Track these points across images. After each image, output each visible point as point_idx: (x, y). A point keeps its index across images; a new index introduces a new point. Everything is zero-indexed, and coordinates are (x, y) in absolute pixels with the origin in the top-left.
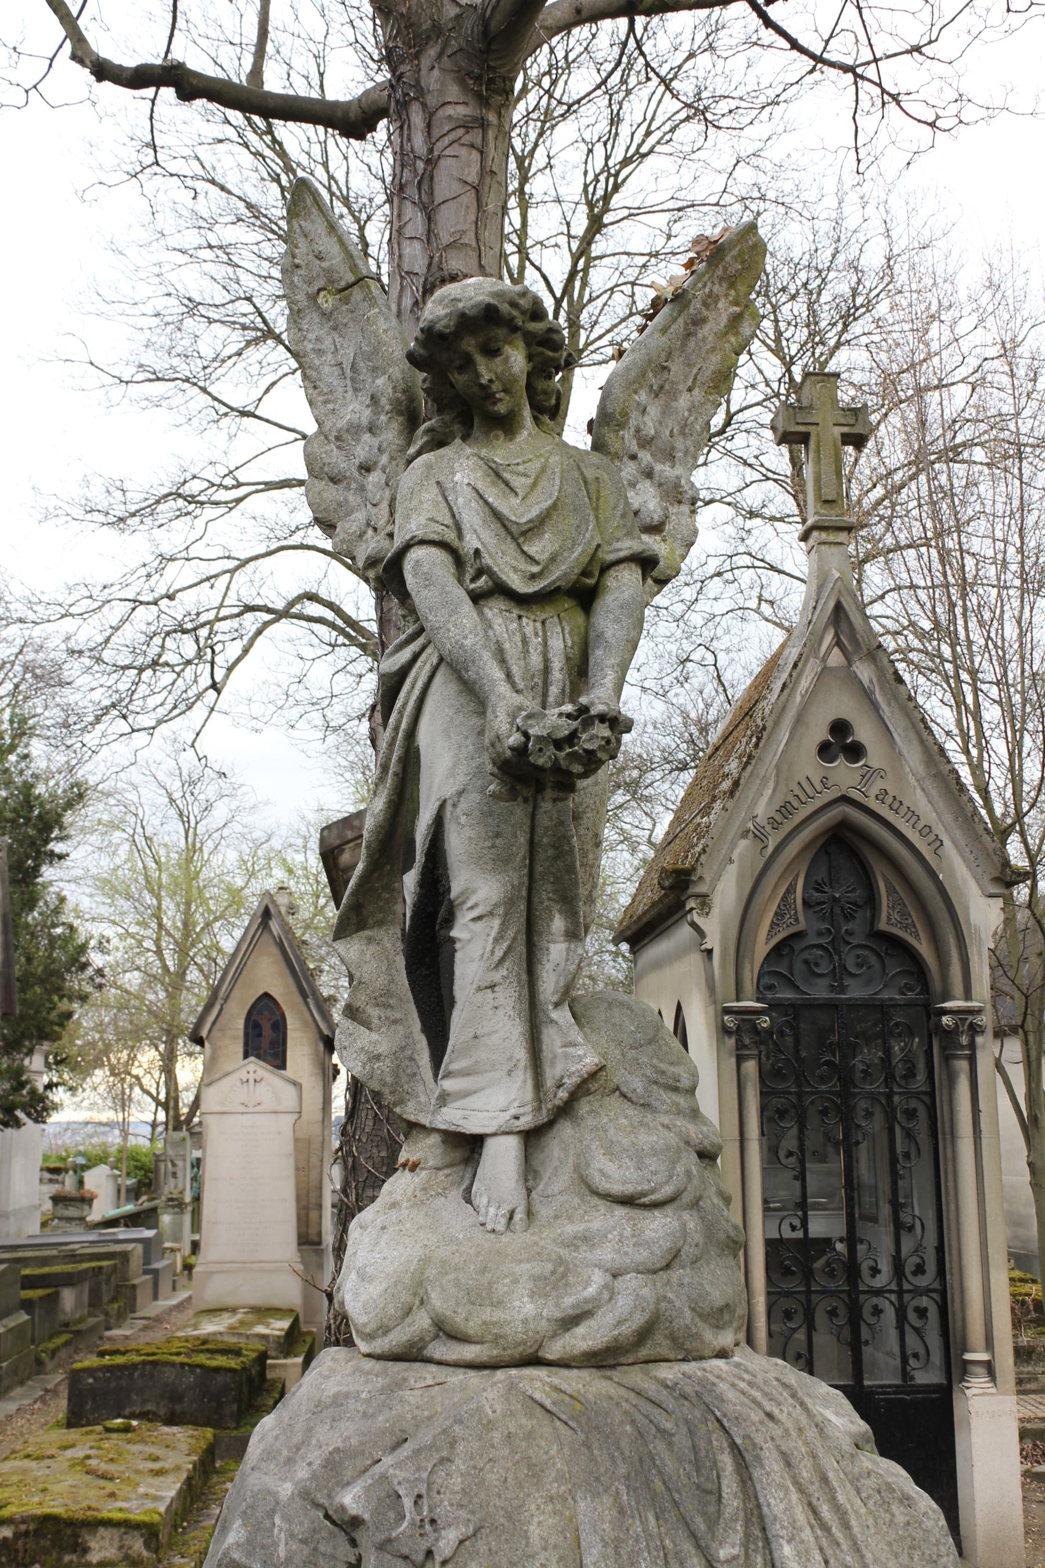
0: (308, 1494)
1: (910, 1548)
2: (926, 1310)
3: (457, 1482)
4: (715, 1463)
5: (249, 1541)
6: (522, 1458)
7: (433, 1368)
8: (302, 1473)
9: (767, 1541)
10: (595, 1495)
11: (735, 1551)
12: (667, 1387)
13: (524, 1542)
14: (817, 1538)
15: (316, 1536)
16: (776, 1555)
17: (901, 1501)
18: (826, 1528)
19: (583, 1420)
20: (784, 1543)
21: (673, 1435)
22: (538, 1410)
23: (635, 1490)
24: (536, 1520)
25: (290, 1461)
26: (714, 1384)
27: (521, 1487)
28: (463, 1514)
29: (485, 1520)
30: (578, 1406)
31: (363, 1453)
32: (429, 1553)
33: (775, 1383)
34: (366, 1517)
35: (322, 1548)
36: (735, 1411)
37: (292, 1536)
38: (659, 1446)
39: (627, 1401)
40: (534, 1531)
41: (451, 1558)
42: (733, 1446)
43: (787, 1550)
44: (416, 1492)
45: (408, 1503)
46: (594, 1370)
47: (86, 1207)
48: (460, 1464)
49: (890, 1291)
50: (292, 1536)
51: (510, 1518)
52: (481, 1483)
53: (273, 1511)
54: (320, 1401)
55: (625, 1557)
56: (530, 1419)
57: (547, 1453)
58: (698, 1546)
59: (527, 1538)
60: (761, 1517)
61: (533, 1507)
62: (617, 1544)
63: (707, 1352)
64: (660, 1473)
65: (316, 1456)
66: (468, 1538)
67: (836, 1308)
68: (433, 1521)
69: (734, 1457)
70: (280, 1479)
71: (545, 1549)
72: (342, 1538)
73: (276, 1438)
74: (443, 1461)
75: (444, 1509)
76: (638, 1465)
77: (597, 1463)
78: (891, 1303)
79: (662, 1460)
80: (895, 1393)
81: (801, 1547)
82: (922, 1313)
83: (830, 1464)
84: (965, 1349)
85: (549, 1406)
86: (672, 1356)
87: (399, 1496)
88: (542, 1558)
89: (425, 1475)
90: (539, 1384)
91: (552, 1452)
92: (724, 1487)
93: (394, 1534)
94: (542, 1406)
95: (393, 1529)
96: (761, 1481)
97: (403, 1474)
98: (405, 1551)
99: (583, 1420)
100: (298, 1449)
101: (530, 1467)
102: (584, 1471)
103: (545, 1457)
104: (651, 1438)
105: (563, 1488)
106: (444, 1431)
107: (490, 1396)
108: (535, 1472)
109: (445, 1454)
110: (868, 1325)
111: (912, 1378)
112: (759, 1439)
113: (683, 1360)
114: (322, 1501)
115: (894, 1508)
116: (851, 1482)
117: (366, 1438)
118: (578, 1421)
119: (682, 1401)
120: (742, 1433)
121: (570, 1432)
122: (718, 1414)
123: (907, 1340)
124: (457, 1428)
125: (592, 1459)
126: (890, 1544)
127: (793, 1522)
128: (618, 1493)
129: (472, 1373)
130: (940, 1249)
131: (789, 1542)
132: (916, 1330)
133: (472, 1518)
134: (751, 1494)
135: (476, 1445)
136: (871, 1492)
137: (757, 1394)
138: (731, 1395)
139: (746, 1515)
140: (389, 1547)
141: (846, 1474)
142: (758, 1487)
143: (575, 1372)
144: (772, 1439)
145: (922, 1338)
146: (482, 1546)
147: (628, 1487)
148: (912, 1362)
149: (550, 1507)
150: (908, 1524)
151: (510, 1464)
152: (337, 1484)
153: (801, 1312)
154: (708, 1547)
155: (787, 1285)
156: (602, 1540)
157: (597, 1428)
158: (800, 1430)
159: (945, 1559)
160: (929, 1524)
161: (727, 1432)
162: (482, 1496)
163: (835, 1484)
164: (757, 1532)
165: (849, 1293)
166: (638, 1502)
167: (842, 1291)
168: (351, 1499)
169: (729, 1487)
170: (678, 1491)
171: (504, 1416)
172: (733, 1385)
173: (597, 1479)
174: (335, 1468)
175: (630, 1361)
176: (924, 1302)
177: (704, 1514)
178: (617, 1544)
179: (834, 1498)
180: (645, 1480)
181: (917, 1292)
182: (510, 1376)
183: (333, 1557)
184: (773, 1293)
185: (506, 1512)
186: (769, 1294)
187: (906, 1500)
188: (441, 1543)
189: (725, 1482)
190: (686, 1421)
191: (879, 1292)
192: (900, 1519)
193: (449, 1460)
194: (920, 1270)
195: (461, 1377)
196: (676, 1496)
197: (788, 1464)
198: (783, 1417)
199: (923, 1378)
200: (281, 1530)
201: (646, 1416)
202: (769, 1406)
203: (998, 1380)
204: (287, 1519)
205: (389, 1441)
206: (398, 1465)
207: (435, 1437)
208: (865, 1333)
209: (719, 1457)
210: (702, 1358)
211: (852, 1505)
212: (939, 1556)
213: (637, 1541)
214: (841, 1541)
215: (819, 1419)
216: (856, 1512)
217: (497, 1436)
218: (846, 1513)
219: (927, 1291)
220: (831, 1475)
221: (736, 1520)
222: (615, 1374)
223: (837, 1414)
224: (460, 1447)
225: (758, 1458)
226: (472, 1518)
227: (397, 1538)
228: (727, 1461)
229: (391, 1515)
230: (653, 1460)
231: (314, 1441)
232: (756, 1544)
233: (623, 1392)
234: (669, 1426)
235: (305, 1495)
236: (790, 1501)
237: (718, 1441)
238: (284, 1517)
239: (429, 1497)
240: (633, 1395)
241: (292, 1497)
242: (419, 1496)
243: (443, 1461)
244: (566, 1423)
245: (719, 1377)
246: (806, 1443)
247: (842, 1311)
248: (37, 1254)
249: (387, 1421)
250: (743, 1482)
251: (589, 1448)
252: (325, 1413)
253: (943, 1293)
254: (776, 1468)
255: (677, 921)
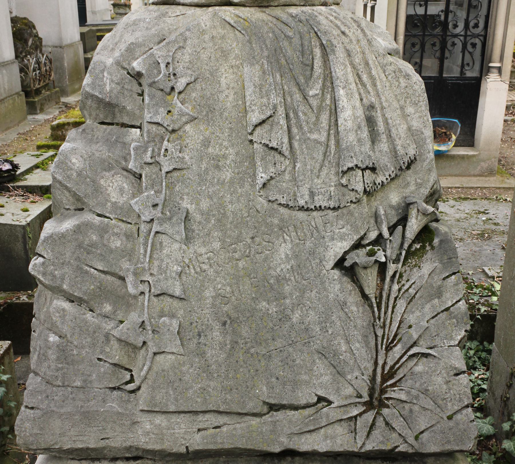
0: (119, 63)
1: (406, 98)
2: (476, 44)
3: (187, 58)
4: (312, 52)
5: (93, 83)
6: (219, 48)
7: (180, 7)
8: (117, 54)
9: (333, 88)
10: (252, 65)
11: (317, 92)
12: (293, 16)
13: (218, 85)
14: (358, 89)
15: (123, 82)
16: (336, 94)
17: (405, 77)
18: (364, 85)
19: (249, 30)
20: (341, 89)
21: (292, 38)
22: (228, 26)
23: (271, 63)
24: (224, 76)
25: (113, 49)
26: (316, 16)
27: (218, 61)
28: (189, 72)
29: (200, 75)
30: (247, 24)
31: (144, 45)
32: (173, 89)
33: (350, 19)
34: (144, 72)
35: (126, 87)
36: (325, 29)
37: (112, 81)
38: (285, 44)
39: (271, 22)
40: (223, 81)
41: (183, 91)
42: (322, 45)
43: (342, 92)
44: (167, 61)
45: (163, 66)
46: (257, 8)
47: (128, 9)
48: (188, 50)
49: (461, 35)
50: (112, 81)
51: (212, 75)
52: (198, 58)
53: (103, 71)
54: (127, 24)
55: (264, 93)
56: (224, 30)
57: (231, 46)
58: (300, 89)
59: (220, 84)
60: (331, 77)
61: (223, 70)
62: (261, 87)
63: (317, 2)
64: (284, 56)
65: (123, 47)
66: (191, 83)
67: (435, 43)
68: (174, 75)
69: (322, 50)
70: (108, 57)
71: (228, 89)
72: (135, 82)
73: (109, 41)
74: (180, 48)
75: (180, 69)
76: (273, 52)
77: (254, 50)
78: (461, 40)
79: (286, 50)
80: (456, 80)
81: (349, 92)
82: (474, 45)
83: (371, 58)
84: (490, 62)
85: (232, 23)
86: (298, 3)
87: (159, 63)
88: (226, 92)
89: (171, 54)
90: (229, 13)
91: (233, 46)
92: (315, 64)
93: (156, 80)
94: (229, 24)
95: (156, 77)
96: (333, 61)
97: (161, 53)
98: (161, 87)
99: (249, 30)
100: (116, 44)
101: (222, 52)
102: (248, 54)
103: (230, 48)
104: (281, 39)
105: (238, 62)
106: (181, 34)
107: (204, 19)
108: (225, 54)
109: (181, 44)
110: (449, 50)
111: (465, 74)
112: (335, 42)
113: (303, 6)
114: (126, 66)
115: (401, 80)
116: (382, 67)
117: (146, 38)
118: (246, 31)
119: (299, 23)
120: (326, 39)
121: (242, 36)
122: (316, 29)
123: (465, 57)
124: (187, 33)
125: (252, 48)
126: (396, 96)
127: (347, 81)
128: (263, 64)
129: (198, 9)
130: (487, 17)
131: (343, 88)
132: (470, 53)
133: (194, 74)
134: (328, 67)
135: (197, 41)
136: (390, 72)
137: (339, 23)
138: (324, 21)
139: (324, 76)
140: (154, 85)
141: (379, 63)
142: (331, 63)
143: (248, 8)
144: (343, 43)
145: (472, 57)
146: (198, 86)
147: (268, 61)
148: (467, 68)
149: (231, 70)
150: (407, 87)
151: (212, 51)
152: (133, 58)
153: (419, 43)
154: (304, 90)
155: (414, 32)
156: (254, 85)
157: (255, 34)
158: (358, 41)
159: (422, 103)
160: (416, 87)
161: (319, 38)
162: (199, 64)
163: (372, 66)
164: (329, 84)
165: (442, 36)
166: (272, 68)
167: (439, 35)
168: (137, 65)
169: (317, 63)
170: (292, 64)
171: (211, 28)
172: (327, 18)
173: (254, 58)
174: (131, 51)
175: (276, 4)
176: (477, 41)
177: (304, 75)
178: (261, 87)
179: (370, 73)
180: (276, 59)
181: (474, 36)
182: (215, 10)
183: (131, 90)
184: (408, 35)
185: (210, 72)
186: (406, 36)
187: (407, 76)
188: (178, 84)
189: (316, 61)
190: (300, 33)
191: (456, 36)
192: (403, 85)
193: (183, 47)
194: (476, 26)
195: (193, 11)
196: (291, 66)
197: (349, 55)
198: (350, 34)
199: (469, 74)
200: (107, 78)
201: (280, 30)
202: (343, 28)
203: (503, 75)
204: (110, 73)
205: (157, 40)
206: (159, 49)
207: (176, 37)
208: (447, 54)
209: (314, 50)
210: (313, 5)
211: (379, 77)
212: (418, 101)
213: (270, 86)
214: (371, 91)
215: (370, 37)
216: (381, 80)
217: (207, 37)
218: (375, 79)
219: (477, 36)
220: (370, 62)
221: (320, 79)
222: (268, 10)
223: (383, 40)
224: (189, 42)
225: (333, 51)
226: (194, 74)
227: (158, 81)
228: (318, 52)
229: (155, 71)
230: (282, 50)
231: (123, 40)
232: (328, 89)
233: (270, 18)
234: (290, 34)
235: (118, 63)
236: (346, 71)
237: (315, 42)
238: (108, 73)
239: (173, 63)
240: (275, 20)
241: (112, 64)
242: (168, 63)
243: (180, 48)
244: (240, 32)
245: (320, 14)
246: (360, 47)
247: (438, 44)
248: (107, 27)
249: (156, 30)
250: (325, 61)
251: (250, 43)
252: (129, 28)
253: (485, 37)
254: (342, 56)
255: (496, 17)
